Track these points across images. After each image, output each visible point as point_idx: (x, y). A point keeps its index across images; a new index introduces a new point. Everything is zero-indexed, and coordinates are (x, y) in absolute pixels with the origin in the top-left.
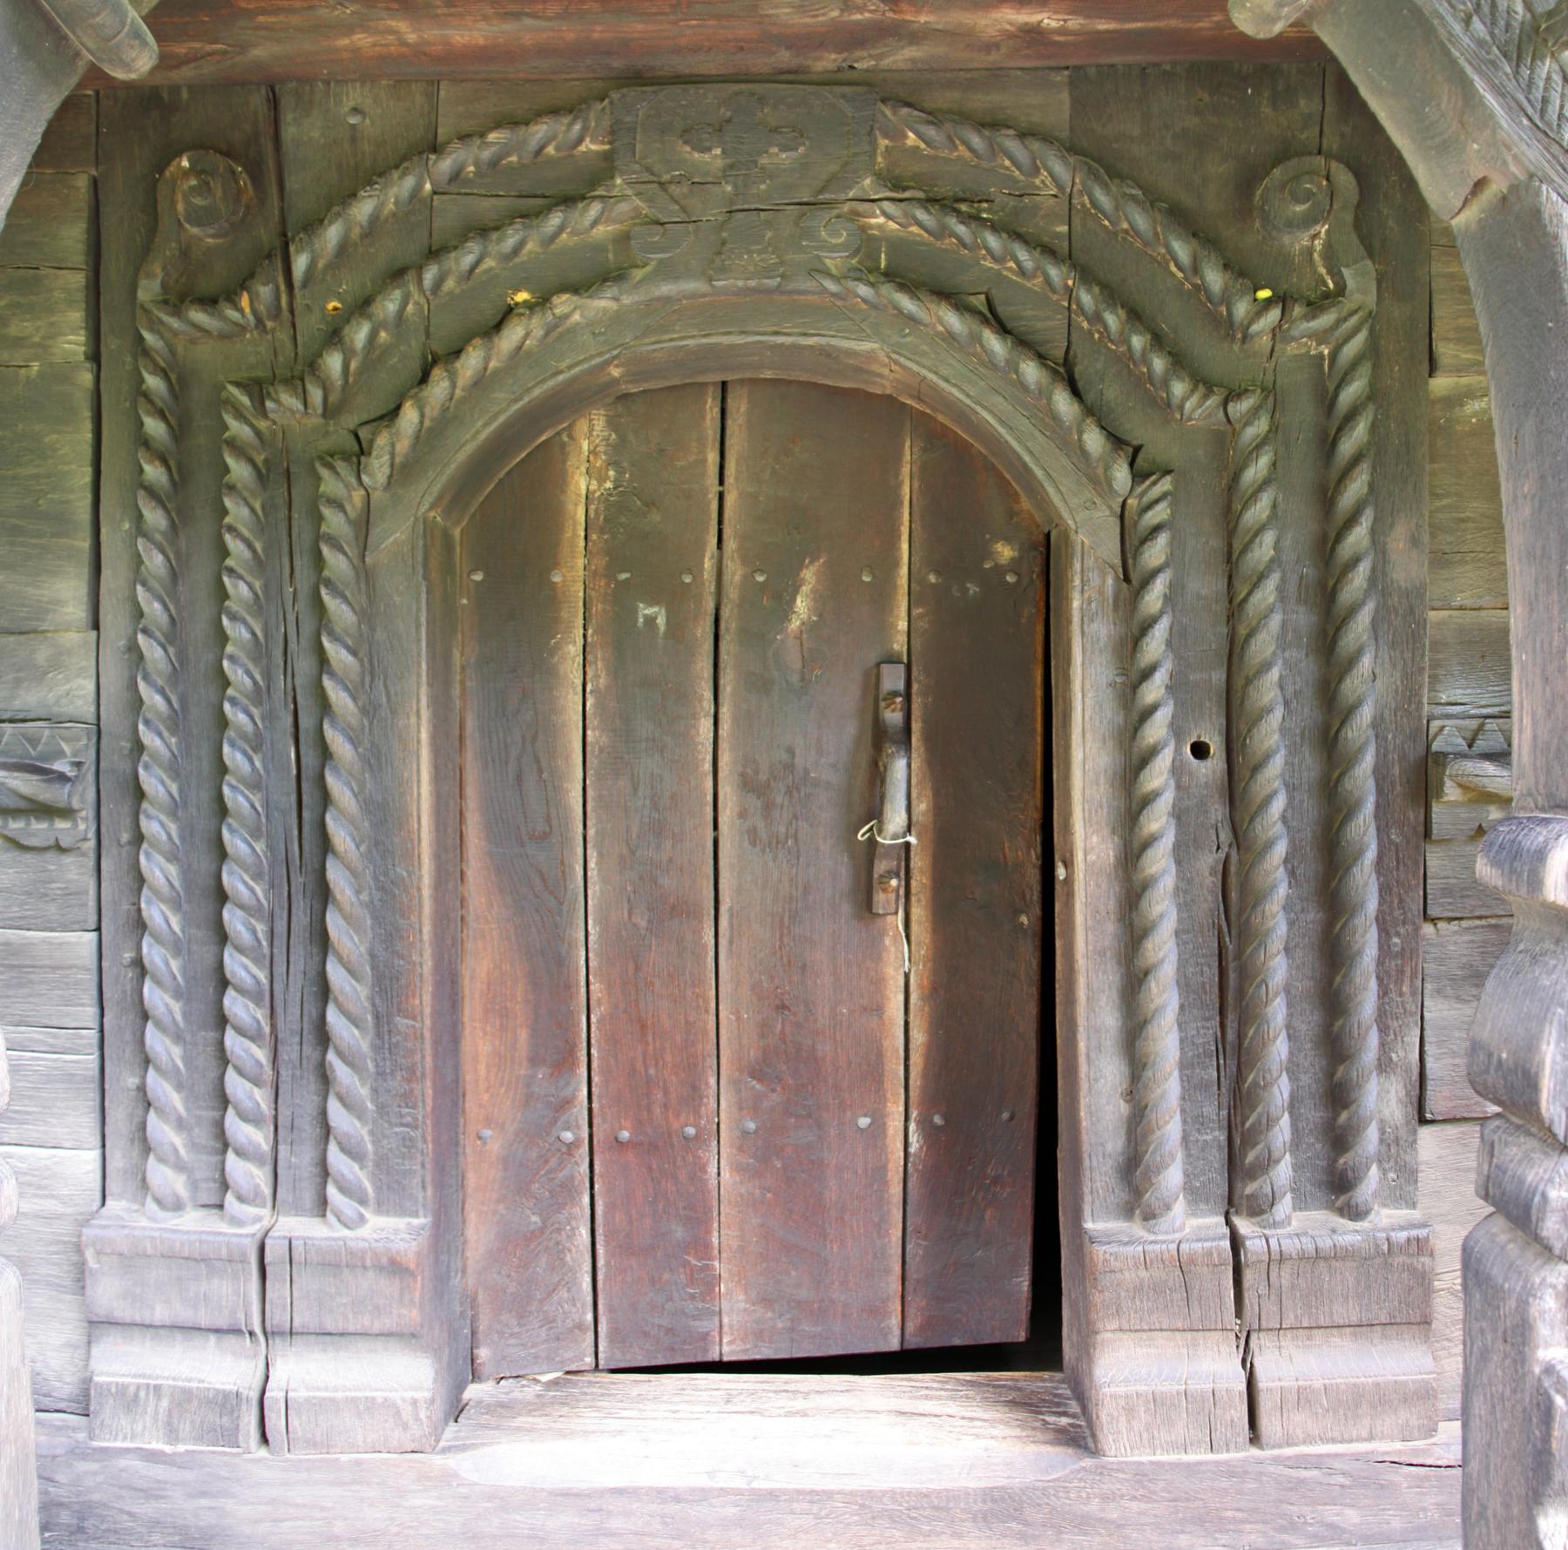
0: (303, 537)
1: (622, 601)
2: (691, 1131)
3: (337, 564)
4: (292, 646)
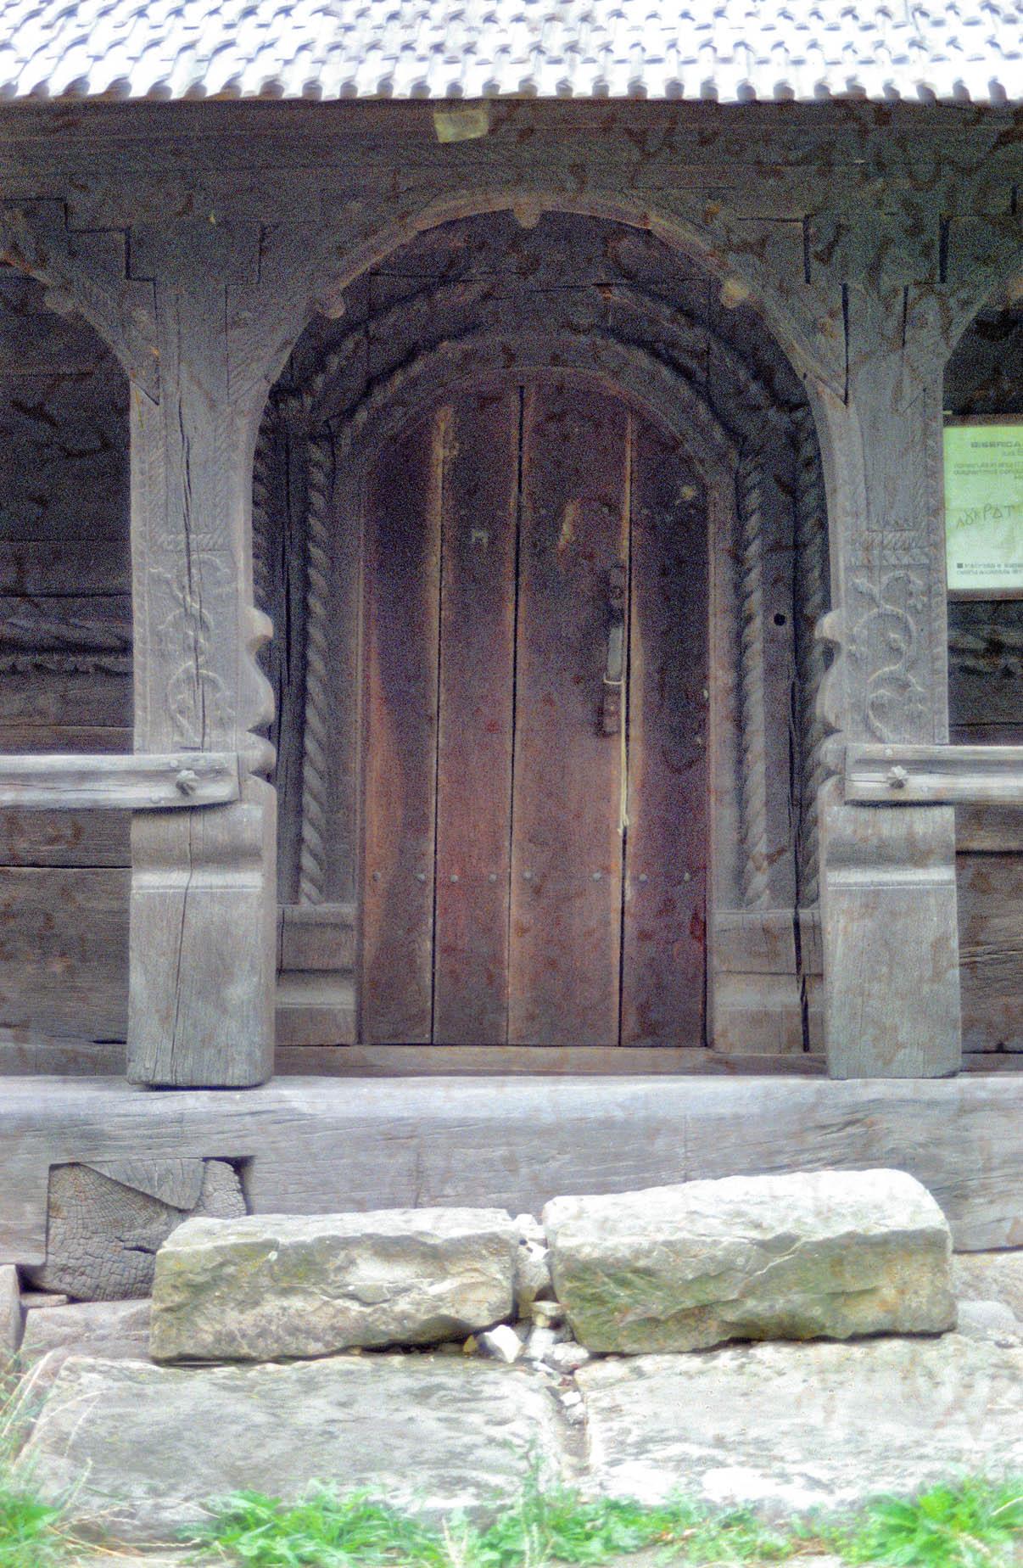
0: (296, 509)
1: (465, 525)
2: (493, 877)
3: (318, 501)
4: (288, 550)
